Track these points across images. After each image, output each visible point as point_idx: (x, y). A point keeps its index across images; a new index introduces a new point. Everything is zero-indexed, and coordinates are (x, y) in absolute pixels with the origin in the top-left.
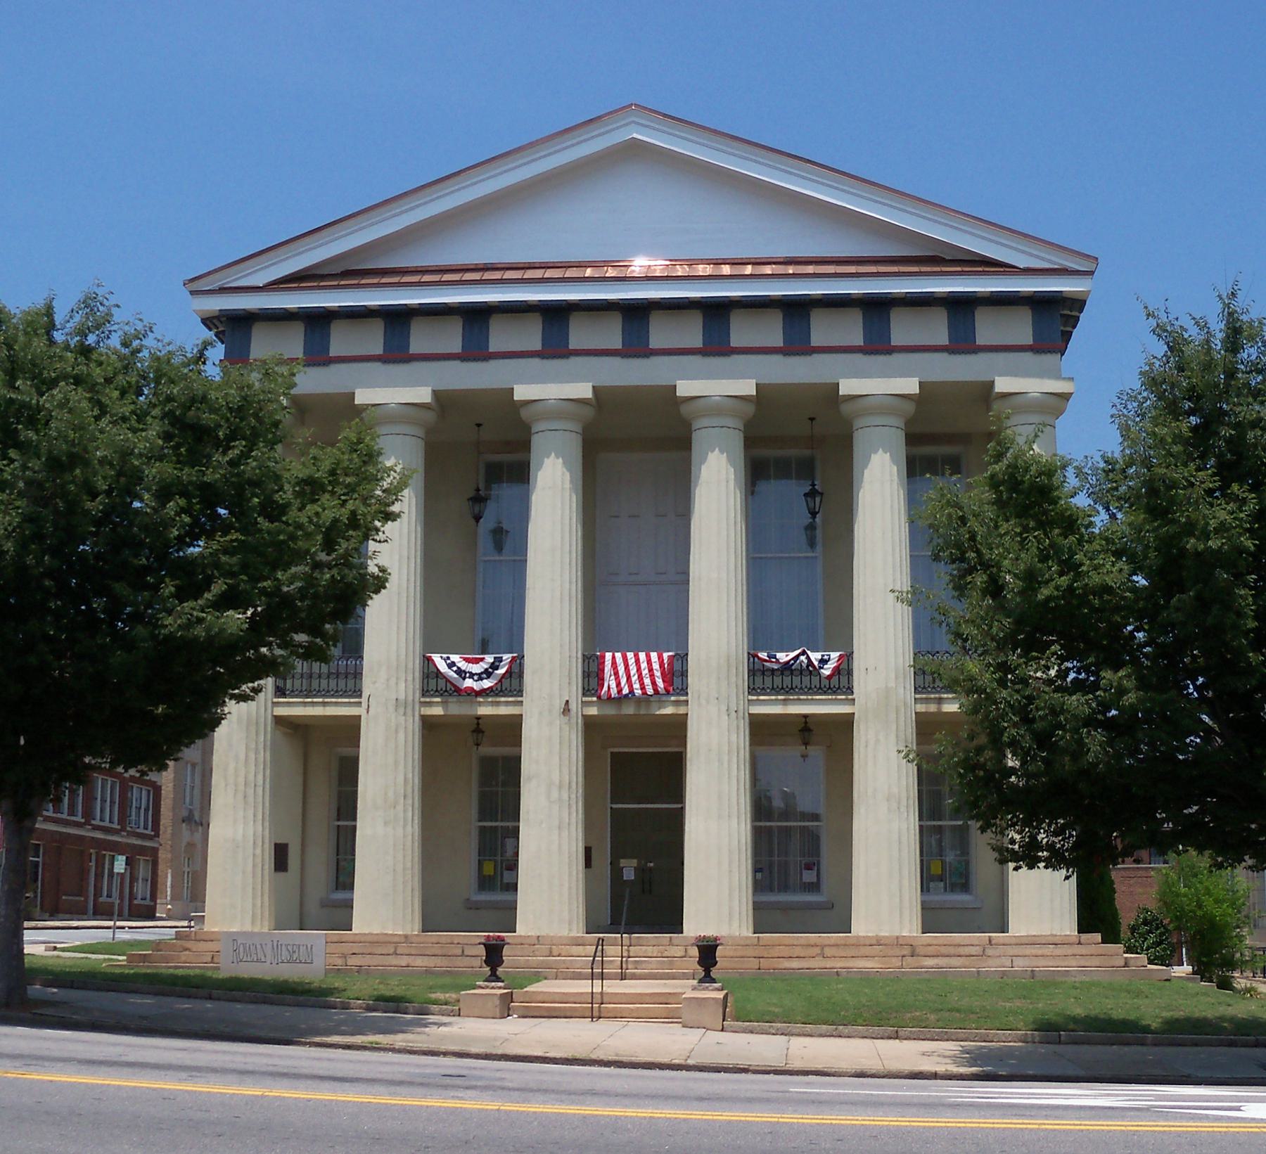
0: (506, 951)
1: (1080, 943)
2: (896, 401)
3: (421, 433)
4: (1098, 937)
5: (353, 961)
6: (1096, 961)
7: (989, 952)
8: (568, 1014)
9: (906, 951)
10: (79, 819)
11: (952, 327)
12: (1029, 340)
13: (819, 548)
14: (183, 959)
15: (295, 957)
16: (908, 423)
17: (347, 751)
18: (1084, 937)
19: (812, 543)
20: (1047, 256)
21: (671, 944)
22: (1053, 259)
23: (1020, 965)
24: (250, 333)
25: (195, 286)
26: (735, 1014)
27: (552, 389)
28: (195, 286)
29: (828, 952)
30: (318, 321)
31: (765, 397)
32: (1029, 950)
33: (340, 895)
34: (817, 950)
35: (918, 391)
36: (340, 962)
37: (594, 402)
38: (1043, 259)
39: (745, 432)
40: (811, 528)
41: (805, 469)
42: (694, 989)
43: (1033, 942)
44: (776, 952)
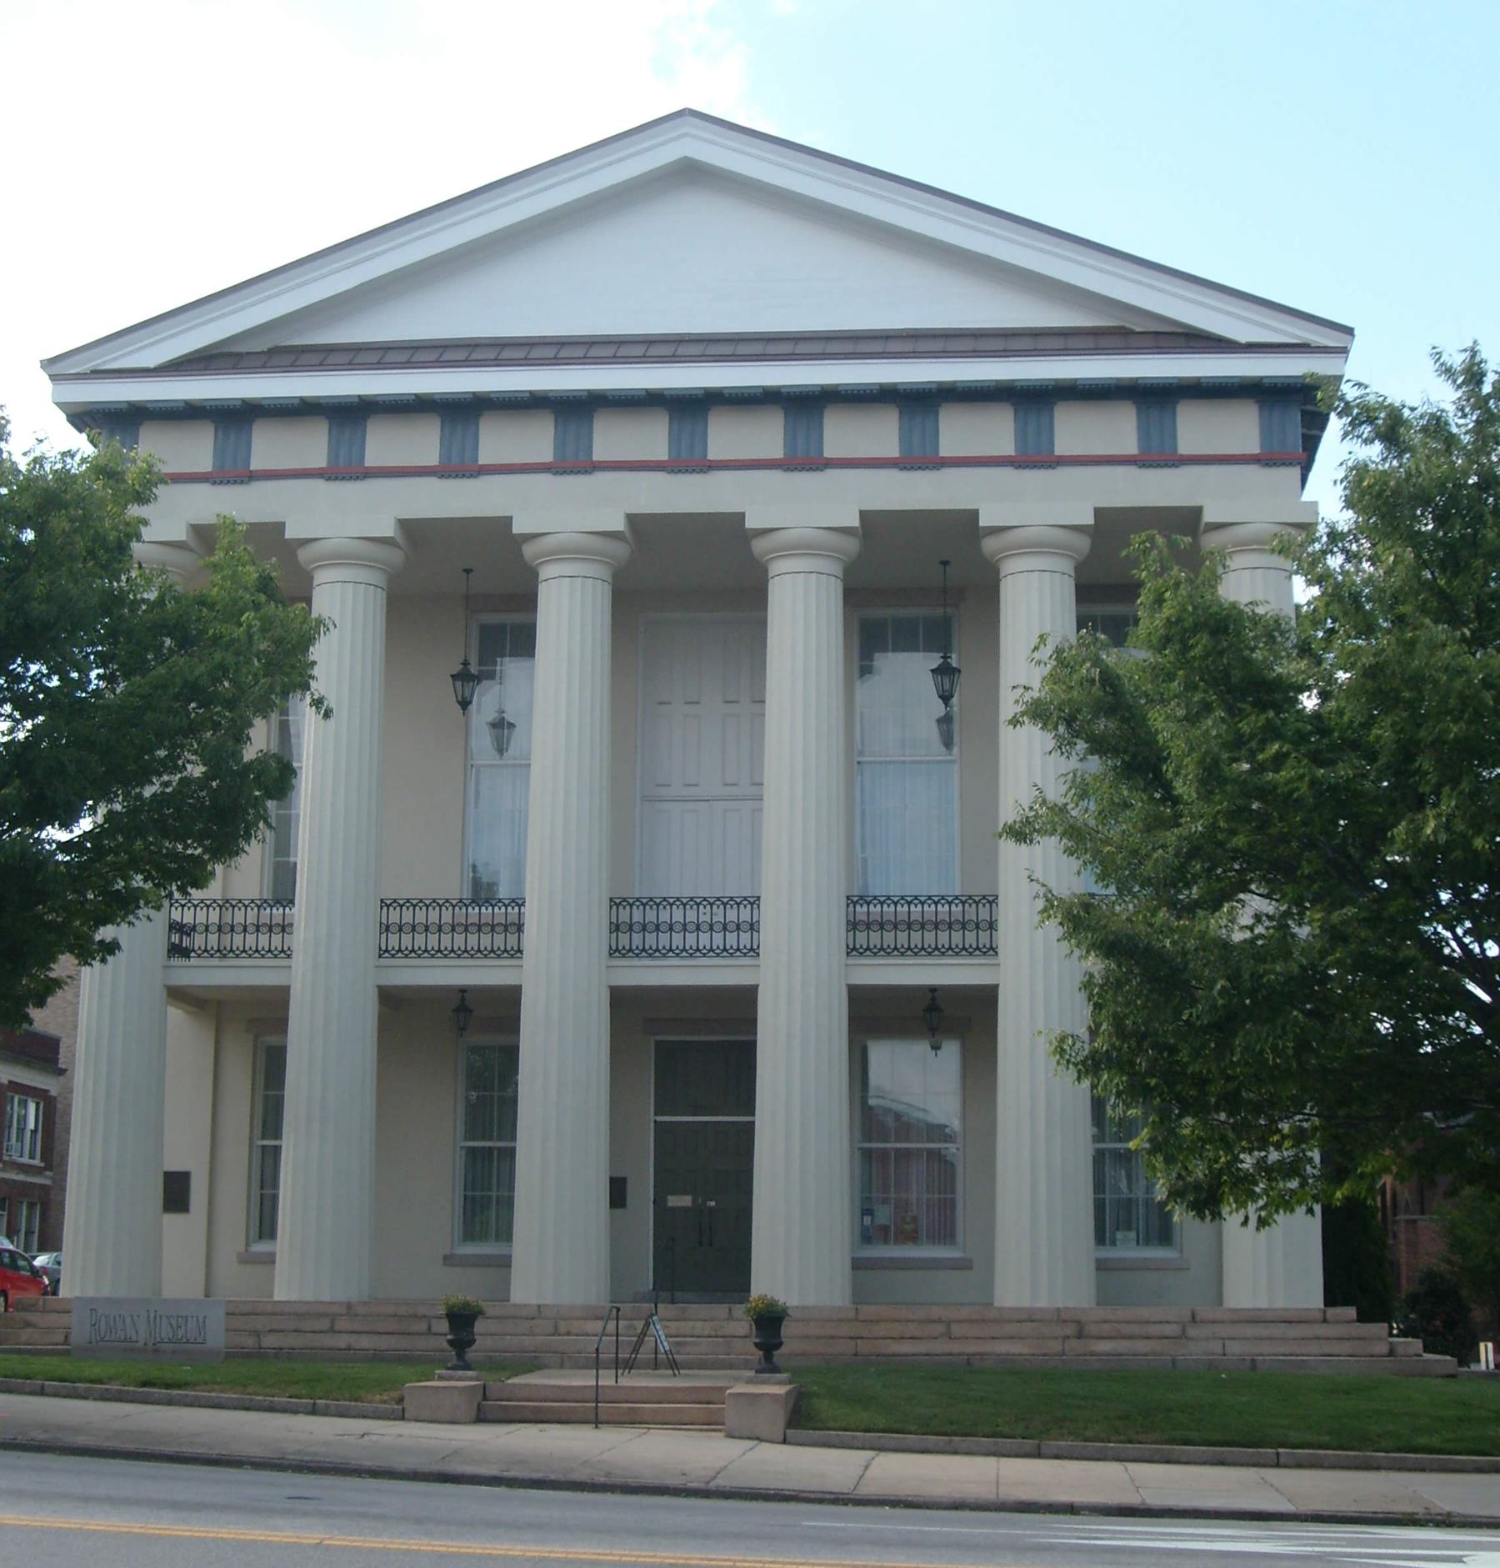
0: (479, 1326)
1: (1325, 1321)
2: (599, 543)
3: (837, 569)
4: (1351, 1312)
5: (270, 1341)
6: (1345, 1347)
7: (1192, 1332)
8: (564, 1417)
9: (1070, 1330)
10: (37, 1162)
11: (674, 440)
12: (1254, 448)
13: (956, 750)
14: (24, 1338)
15: (181, 1333)
16: (1079, 569)
17: (272, 1040)
18: (1333, 1312)
19: (948, 742)
20: (1283, 327)
21: (730, 1317)
22: (1290, 329)
23: (1234, 1348)
24: (137, 435)
25: (59, 369)
26: (802, 1420)
27: (569, 514)
28: (58, 368)
29: (956, 1329)
30: (235, 418)
31: (875, 526)
32: (1249, 1330)
33: (261, 1247)
34: (939, 1329)
35: (1092, 522)
36: (250, 1342)
37: (400, 539)
38: (1275, 330)
39: (845, 581)
40: (945, 721)
41: (937, 636)
42: (750, 1381)
43: (1255, 1318)
44: (881, 1330)
